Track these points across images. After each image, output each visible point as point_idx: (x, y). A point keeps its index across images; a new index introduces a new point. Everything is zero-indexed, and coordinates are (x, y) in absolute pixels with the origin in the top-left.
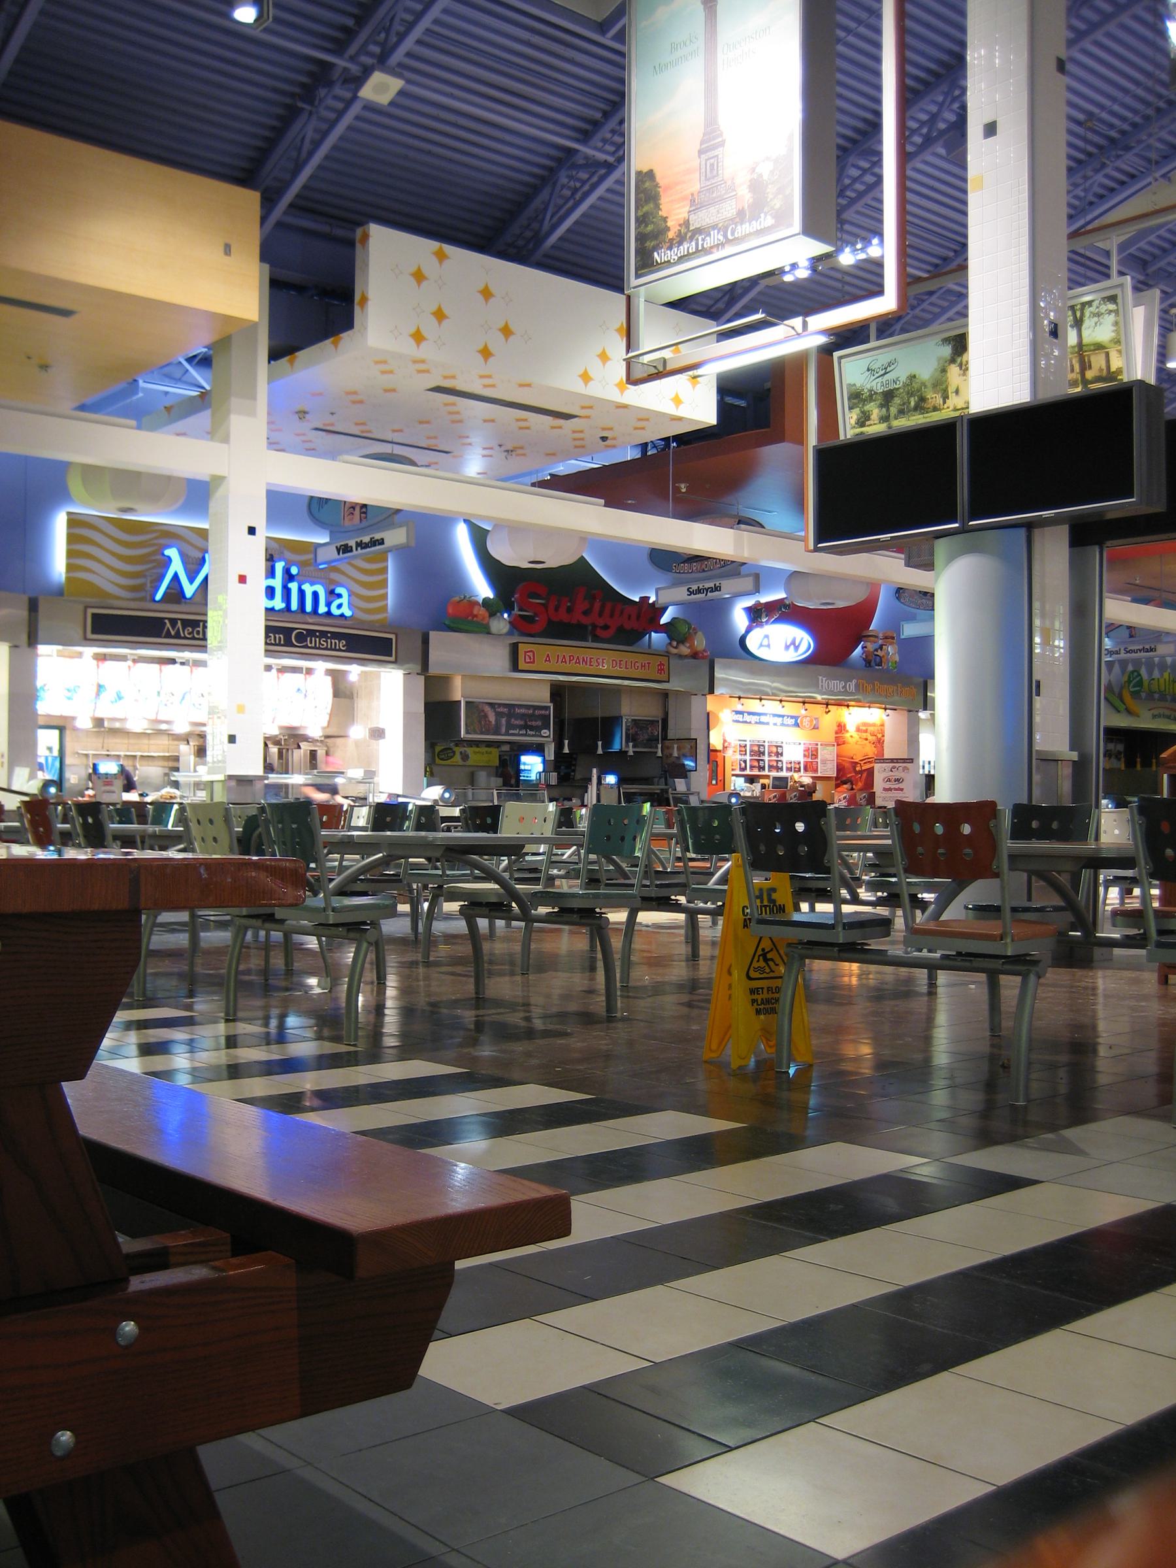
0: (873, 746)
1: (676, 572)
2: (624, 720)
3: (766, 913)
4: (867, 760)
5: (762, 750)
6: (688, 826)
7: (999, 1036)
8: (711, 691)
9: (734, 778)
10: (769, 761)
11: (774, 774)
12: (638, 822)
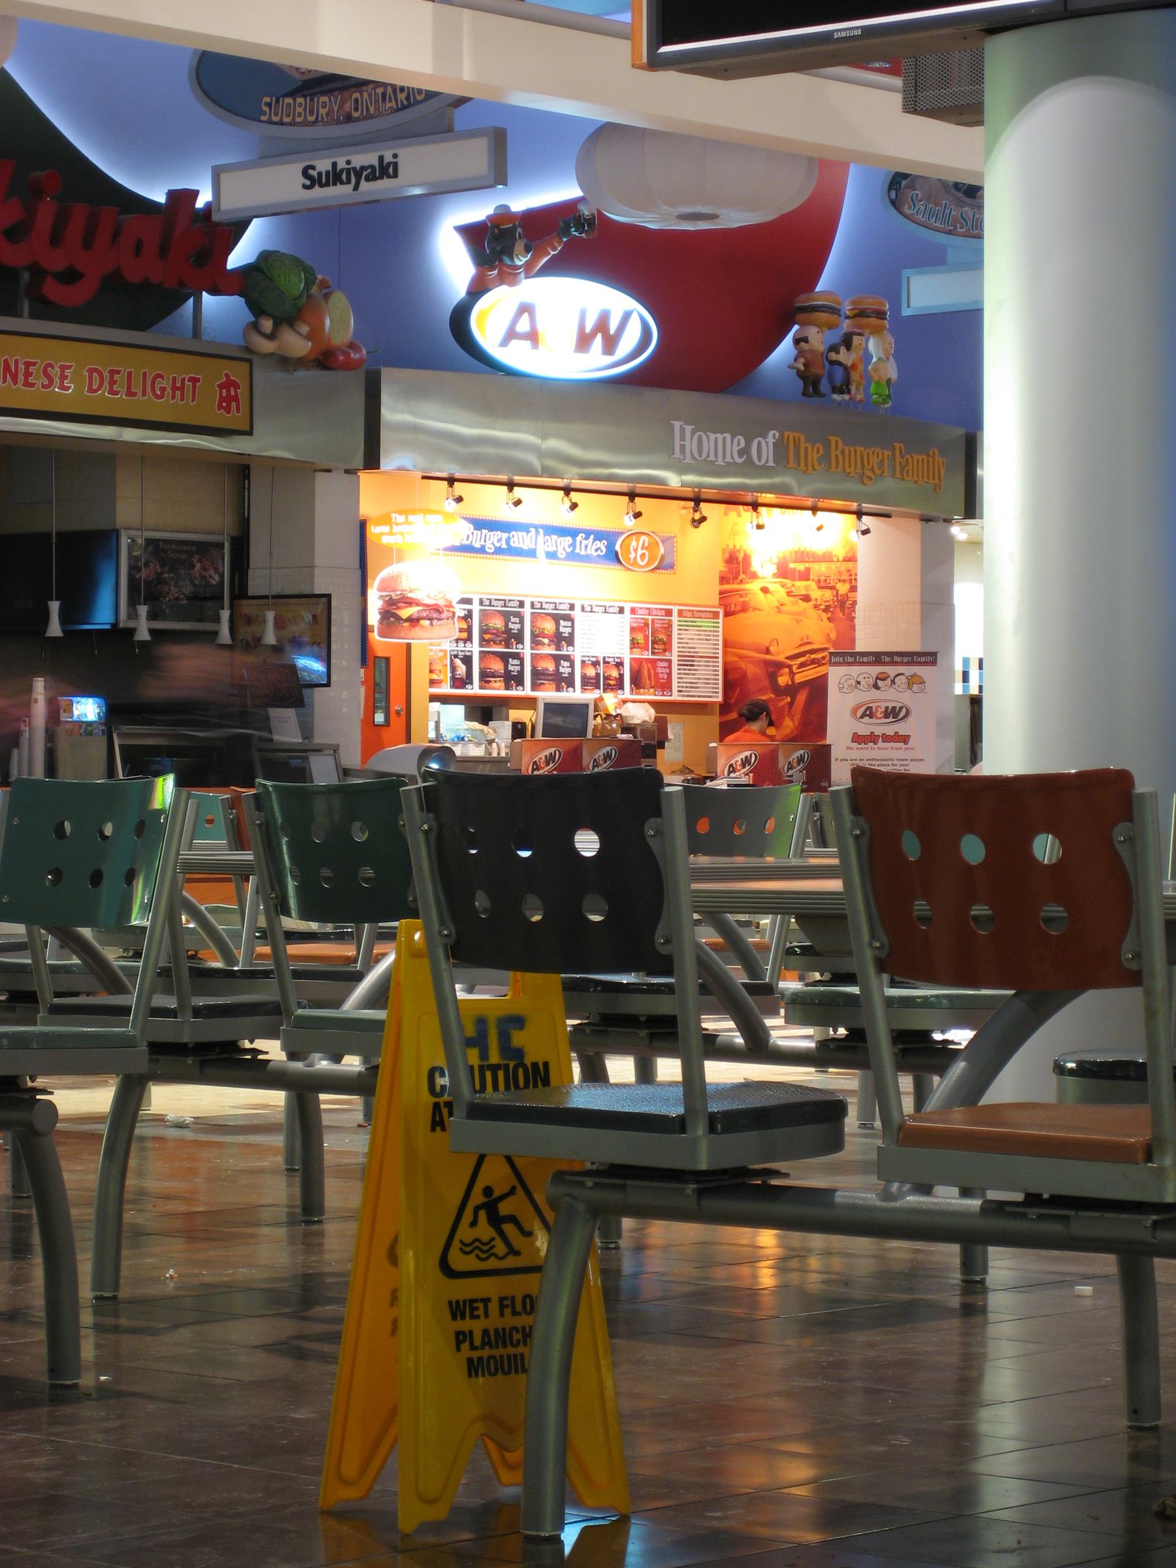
0: (824, 616)
1: (271, 122)
2: (124, 542)
3: (496, 1087)
4: (808, 656)
5: (515, 627)
6: (285, 840)
7: (1155, 1429)
8: (372, 461)
9: (435, 706)
10: (534, 657)
11: (548, 695)
12: (140, 828)
